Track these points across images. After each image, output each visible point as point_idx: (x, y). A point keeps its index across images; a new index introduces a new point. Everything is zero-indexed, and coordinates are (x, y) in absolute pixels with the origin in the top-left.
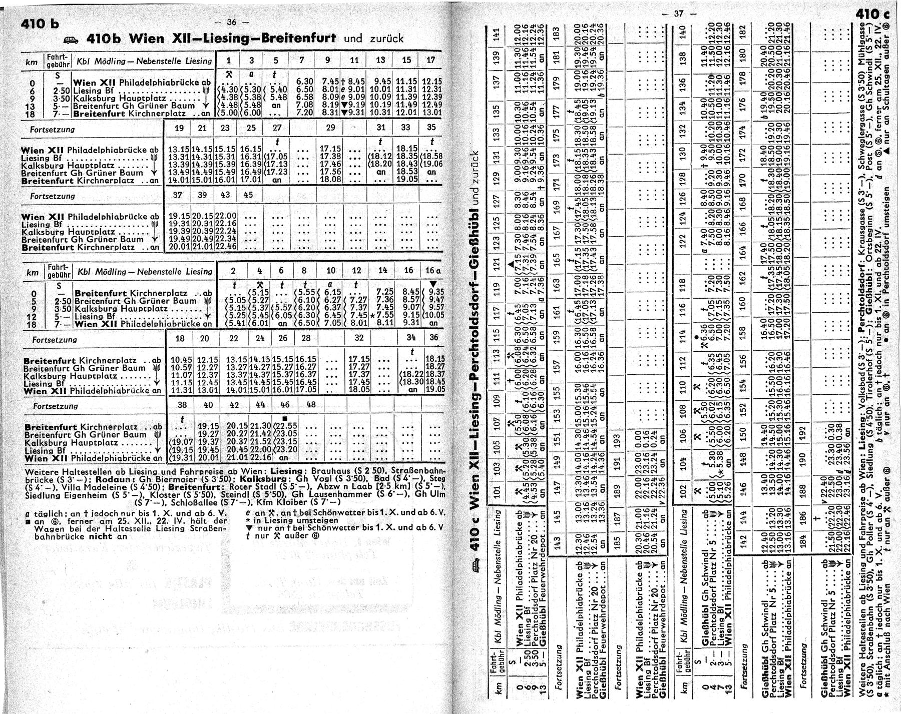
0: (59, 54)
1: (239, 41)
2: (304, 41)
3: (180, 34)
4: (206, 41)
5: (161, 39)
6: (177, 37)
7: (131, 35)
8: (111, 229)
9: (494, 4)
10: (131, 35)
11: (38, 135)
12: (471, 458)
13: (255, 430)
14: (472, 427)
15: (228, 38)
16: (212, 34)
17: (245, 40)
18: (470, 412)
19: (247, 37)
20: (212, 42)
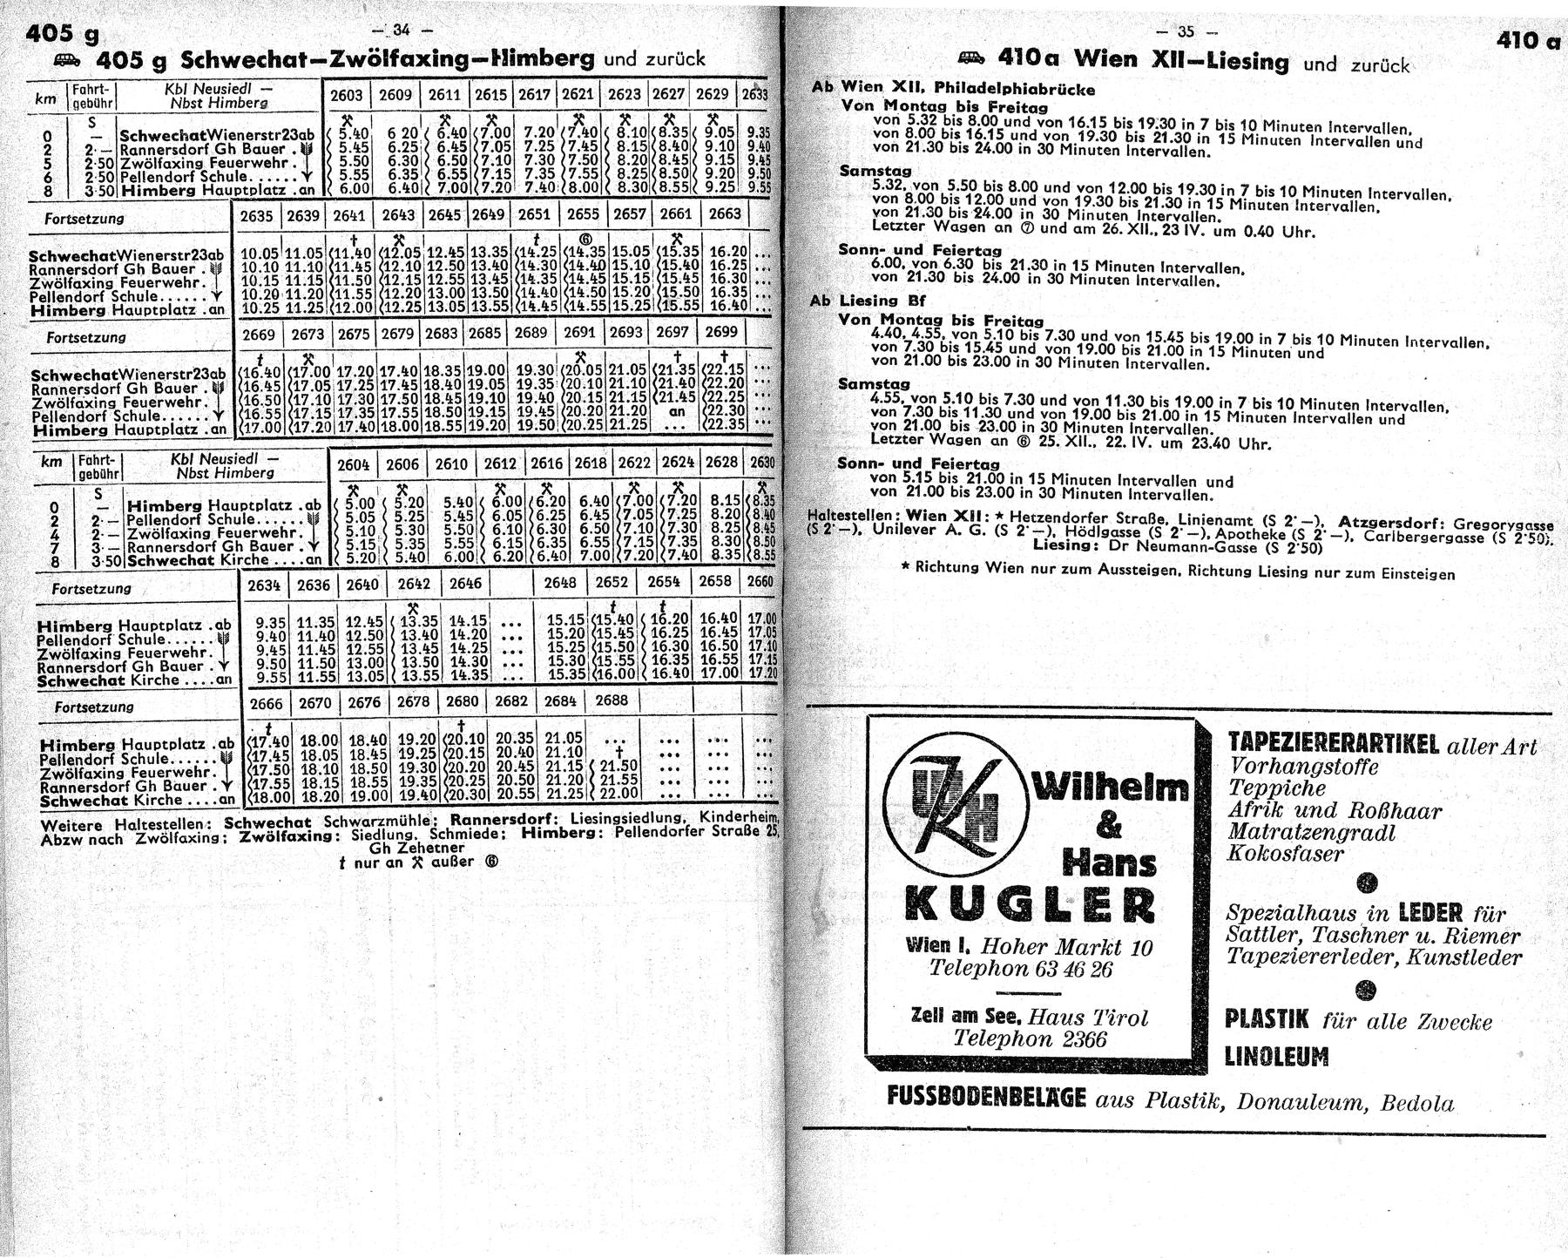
0: (93, 84)
1: (451, 64)
2: (1127, 65)
3: (1165, 52)
4: (1212, 65)
5: (1132, 60)
6: (1160, 56)
7: (1077, 52)
8: (190, 424)
9: (848, 9)
10: (1077, 52)
11: (59, 228)
12: (1174, 53)
13: (554, 774)
14: (1227, 57)
15: (1252, 61)
16: (1223, 53)
17: (462, 62)
18: (435, 51)
19: (466, 57)
20: (1223, 66)
